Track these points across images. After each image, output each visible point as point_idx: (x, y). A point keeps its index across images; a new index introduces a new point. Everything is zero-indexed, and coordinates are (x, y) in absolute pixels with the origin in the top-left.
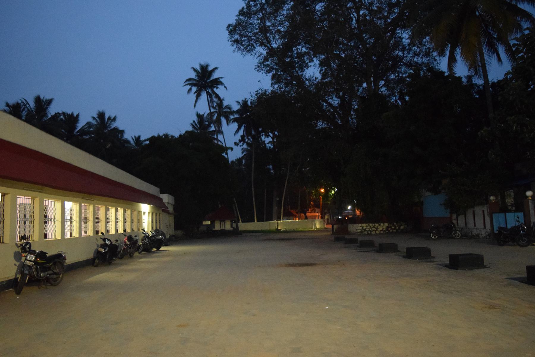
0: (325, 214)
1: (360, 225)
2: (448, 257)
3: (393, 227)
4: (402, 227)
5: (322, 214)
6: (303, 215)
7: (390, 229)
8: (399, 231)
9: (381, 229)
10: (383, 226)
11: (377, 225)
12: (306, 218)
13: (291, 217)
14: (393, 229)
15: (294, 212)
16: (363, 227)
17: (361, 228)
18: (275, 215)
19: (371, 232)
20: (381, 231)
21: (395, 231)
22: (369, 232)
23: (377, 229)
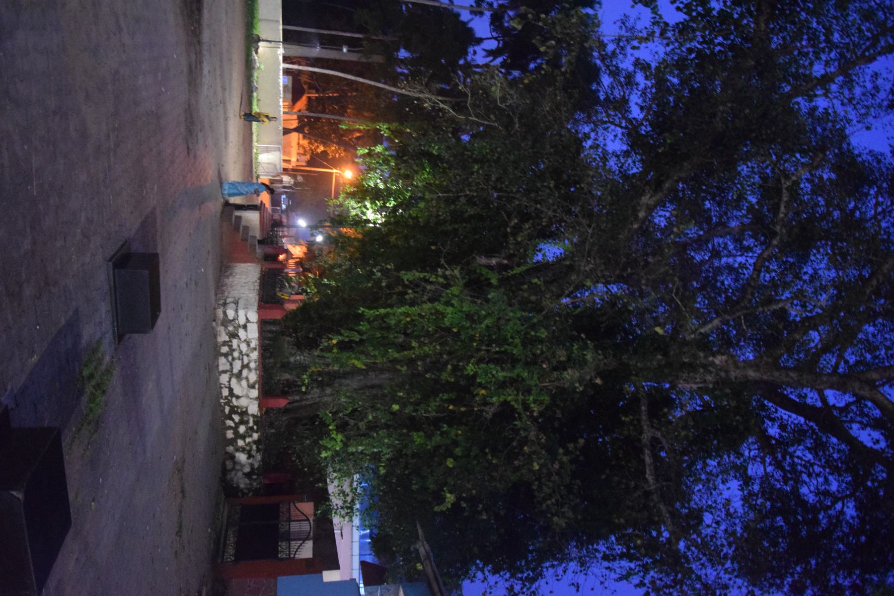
0: (294, 177)
1: (253, 316)
2: (286, 136)
3: (242, 429)
4: (242, 457)
5: (293, 170)
6: (294, 124)
7: (237, 418)
8: (230, 449)
9: (237, 391)
10: (249, 400)
11: (253, 377)
12: (286, 131)
13: (290, 96)
14: (235, 429)
15: (302, 103)
16: (245, 327)
17: (242, 320)
18: (297, 50)
19: (226, 355)
20: (231, 390)
21: (230, 434)
22: (225, 349)
23: (239, 376)
